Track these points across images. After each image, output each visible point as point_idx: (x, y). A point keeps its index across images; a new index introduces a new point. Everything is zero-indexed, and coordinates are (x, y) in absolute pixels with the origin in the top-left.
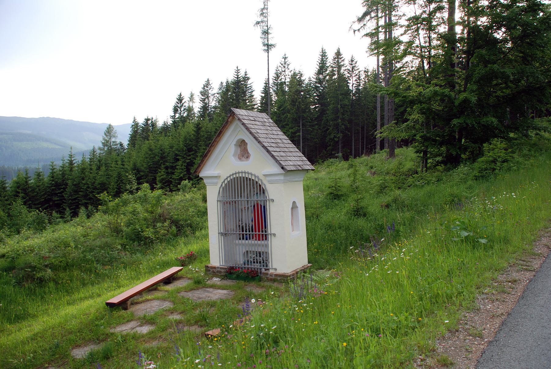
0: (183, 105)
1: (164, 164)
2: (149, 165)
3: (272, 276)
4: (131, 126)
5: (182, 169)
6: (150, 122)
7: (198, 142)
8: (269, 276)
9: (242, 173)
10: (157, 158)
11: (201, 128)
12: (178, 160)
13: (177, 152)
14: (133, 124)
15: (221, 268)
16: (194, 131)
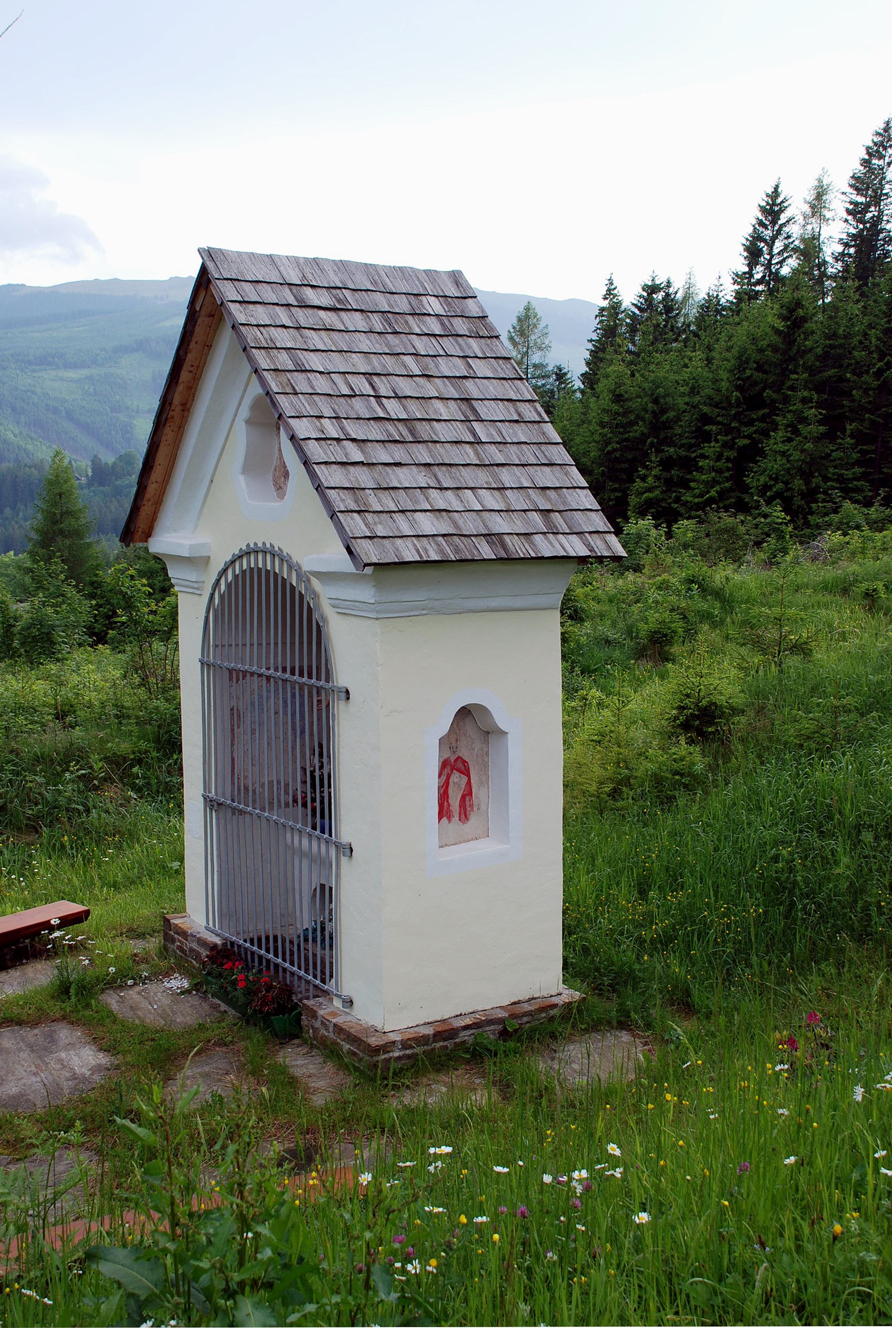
0: (779, 232)
1: (659, 451)
2: (609, 453)
4: (597, 312)
5: (719, 471)
6: (660, 296)
7: (784, 374)
10: (640, 428)
11: (804, 320)
12: (707, 437)
13: (706, 409)
14: (605, 304)
16: (777, 332)
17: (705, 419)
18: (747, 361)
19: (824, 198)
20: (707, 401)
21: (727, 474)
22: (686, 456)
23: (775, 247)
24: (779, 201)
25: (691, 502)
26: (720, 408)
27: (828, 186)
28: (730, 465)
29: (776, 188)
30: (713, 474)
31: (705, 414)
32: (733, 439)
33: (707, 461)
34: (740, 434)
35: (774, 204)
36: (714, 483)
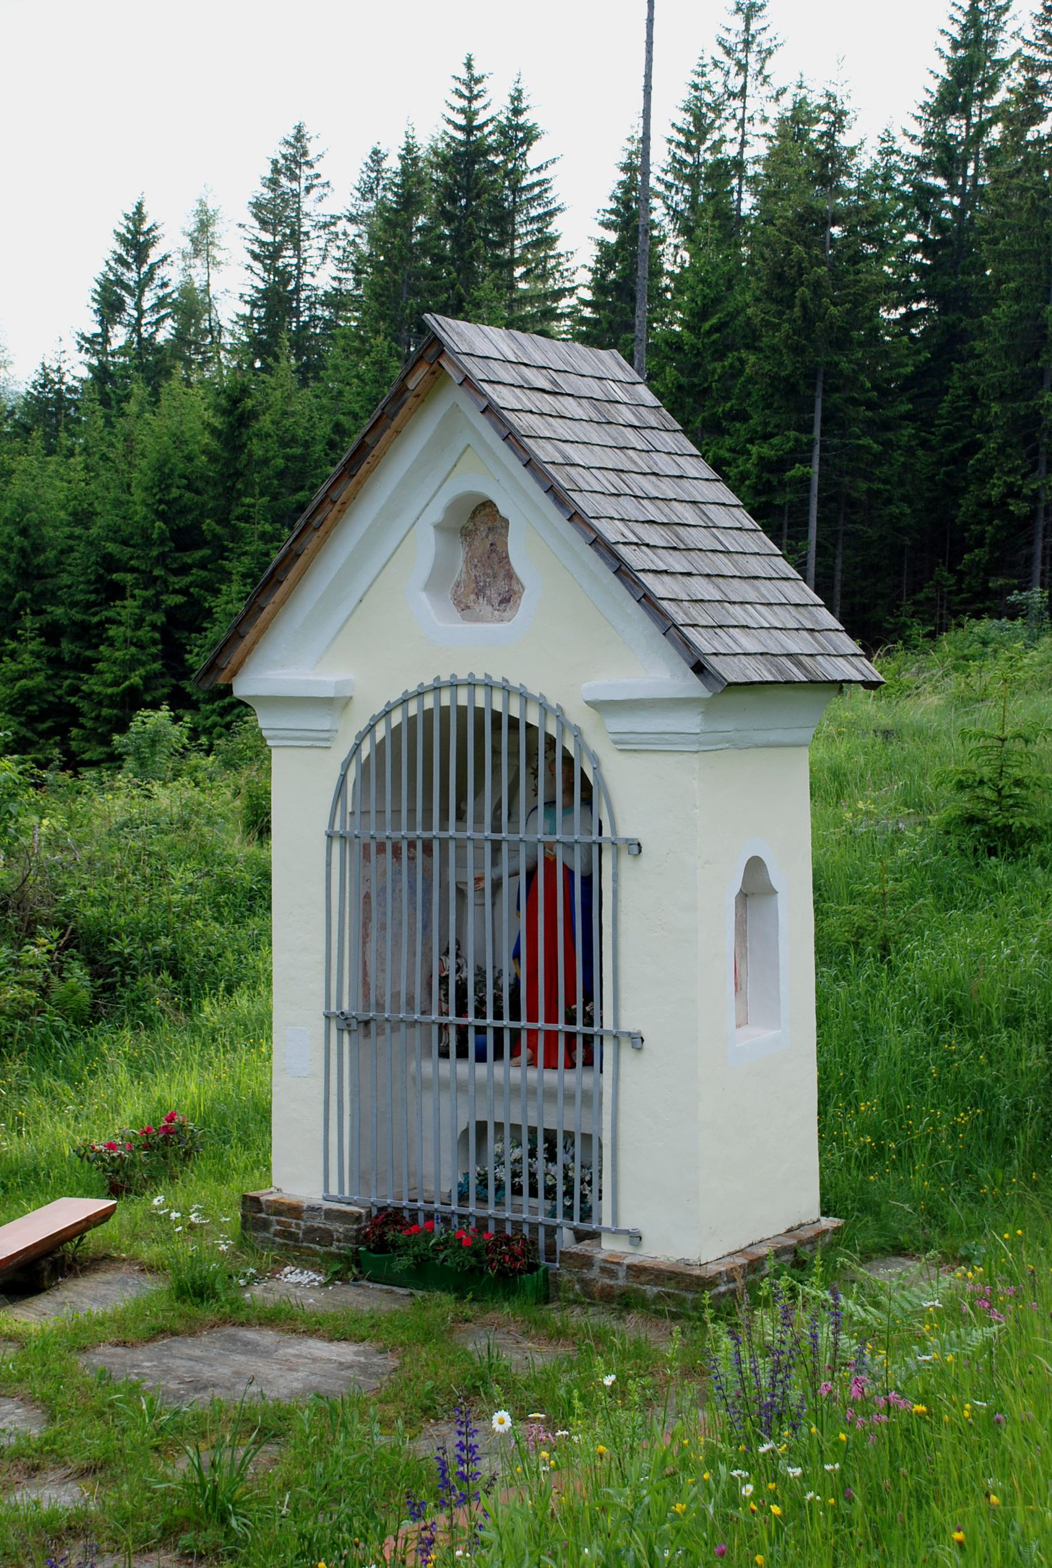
0: (150, 275)
1: (38, 613)
5: (140, 645)
7: (231, 495)
8: (594, 1274)
11: (254, 415)
12: (117, 592)
13: (111, 547)
15: (330, 1214)
17: (110, 563)
18: (170, 475)
19: (211, 229)
20: (111, 534)
21: (153, 650)
22: (83, 622)
23: (144, 299)
24: (145, 227)
25: (99, 693)
26: (133, 546)
27: (215, 212)
28: (157, 635)
29: (139, 207)
30: (133, 649)
31: (110, 555)
32: (157, 594)
33: (122, 629)
34: (167, 587)
35: (137, 232)
36: (132, 664)
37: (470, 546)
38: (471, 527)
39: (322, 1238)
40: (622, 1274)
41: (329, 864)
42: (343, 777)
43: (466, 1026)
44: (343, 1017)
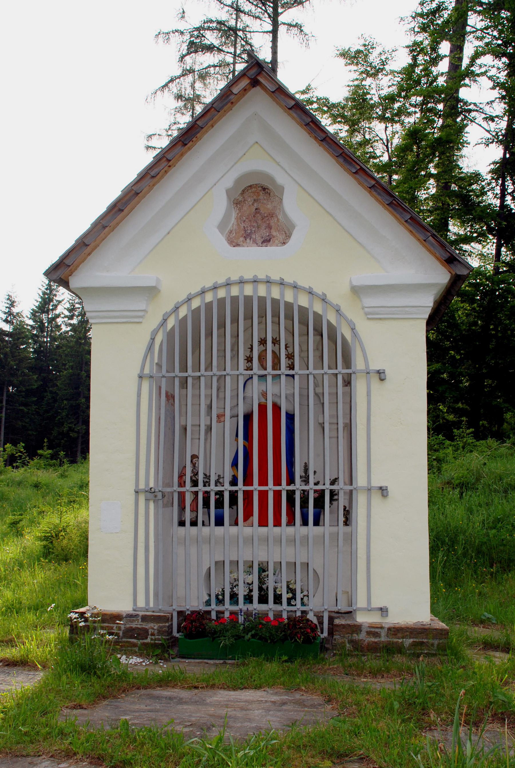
3: (376, 635)
8: (362, 636)
9: (255, 281)
15: (145, 618)
37: (240, 210)
38: (241, 198)
39: (139, 634)
40: (383, 633)
41: (139, 395)
42: (153, 339)
43: (252, 492)
44: (150, 491)
